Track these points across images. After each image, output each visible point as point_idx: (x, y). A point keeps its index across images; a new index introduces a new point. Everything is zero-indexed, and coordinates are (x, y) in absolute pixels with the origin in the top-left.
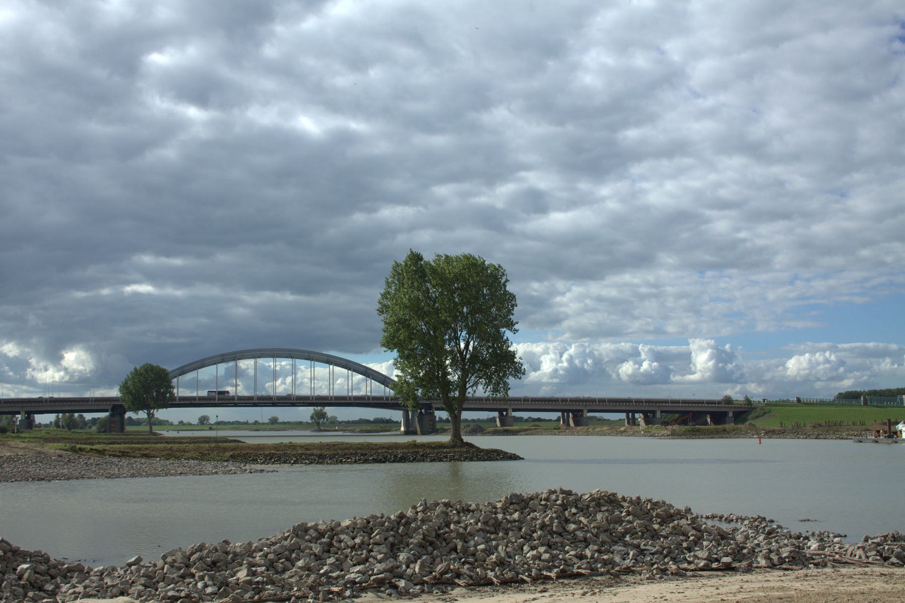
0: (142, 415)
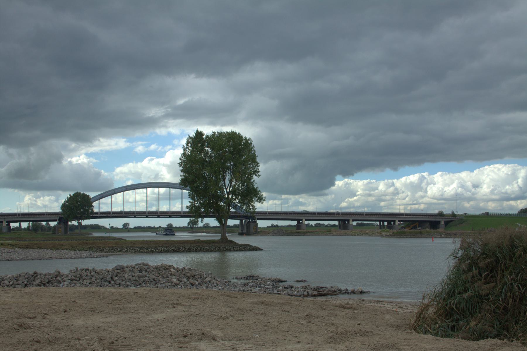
0: (75, 223)
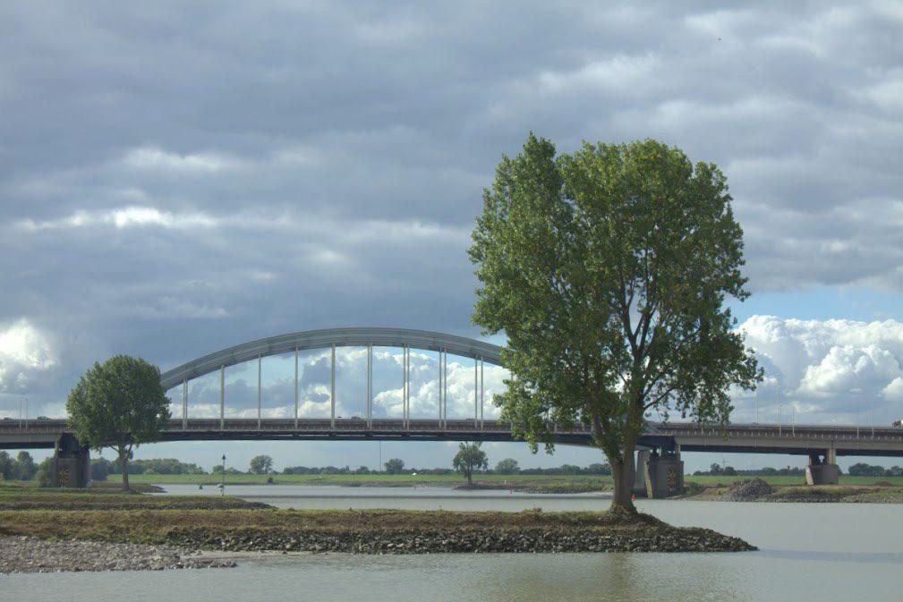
0: (110, 454)
